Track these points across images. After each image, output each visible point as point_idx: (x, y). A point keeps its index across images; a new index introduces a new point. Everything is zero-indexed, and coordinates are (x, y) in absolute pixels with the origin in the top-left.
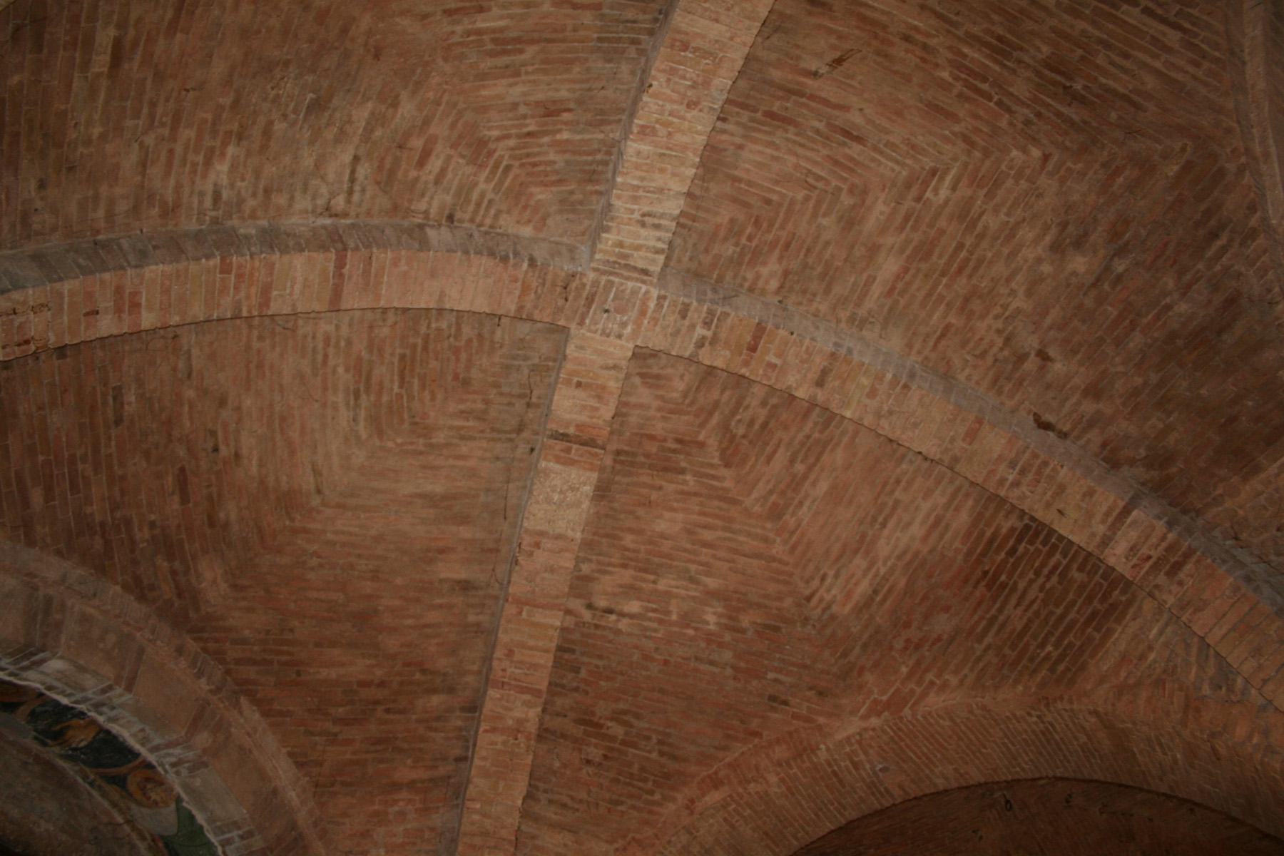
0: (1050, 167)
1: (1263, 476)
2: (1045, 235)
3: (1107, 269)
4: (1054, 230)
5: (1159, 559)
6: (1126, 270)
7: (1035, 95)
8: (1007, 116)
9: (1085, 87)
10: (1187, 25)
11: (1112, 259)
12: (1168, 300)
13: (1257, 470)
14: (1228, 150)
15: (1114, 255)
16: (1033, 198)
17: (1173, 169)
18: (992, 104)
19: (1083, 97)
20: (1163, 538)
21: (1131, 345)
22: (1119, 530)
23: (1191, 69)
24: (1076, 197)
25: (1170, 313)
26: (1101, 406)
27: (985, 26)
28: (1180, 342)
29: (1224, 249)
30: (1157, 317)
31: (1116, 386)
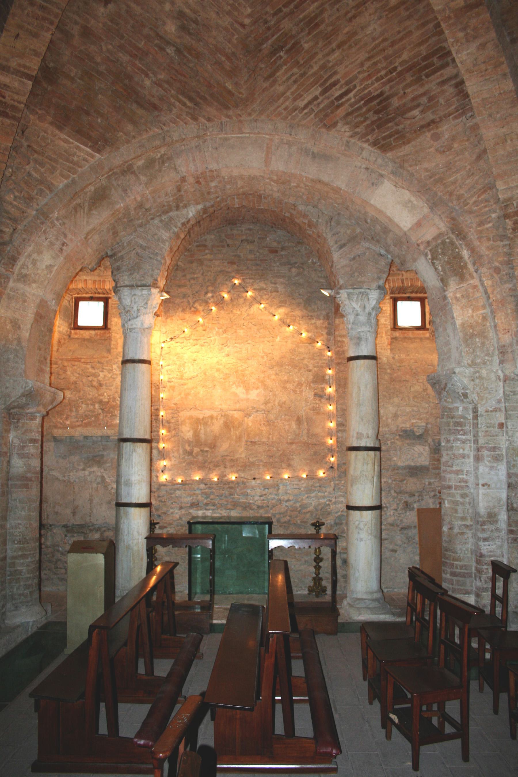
0: (236, 26)
1: (57, 132)
2: (191, 10)
3: (168, 43)
4: (193, 16)
5: (5, 103)
6: (168, 54)
7: (280, 30)
8: (272, 12)
9: (281, 57)
10: (305, 111)
11: (174, 46)
12: (151, 75)
13: (60, 128)
14: (239, 113)
15: (177, 48)
16: (216, 10)
17: (229, 86)
18: (281, 6)
19: (275, 55)
20: (19, 102)
21: (121, 55)
22: (16, 75)
23: (283, 106)
24: (214, 33)
25: (143, 76)
26: (77, 37)
27: (327, 21)
28: (127, 82)
29: (184, 104)
30: (139, 69)
31: (92, 46)
